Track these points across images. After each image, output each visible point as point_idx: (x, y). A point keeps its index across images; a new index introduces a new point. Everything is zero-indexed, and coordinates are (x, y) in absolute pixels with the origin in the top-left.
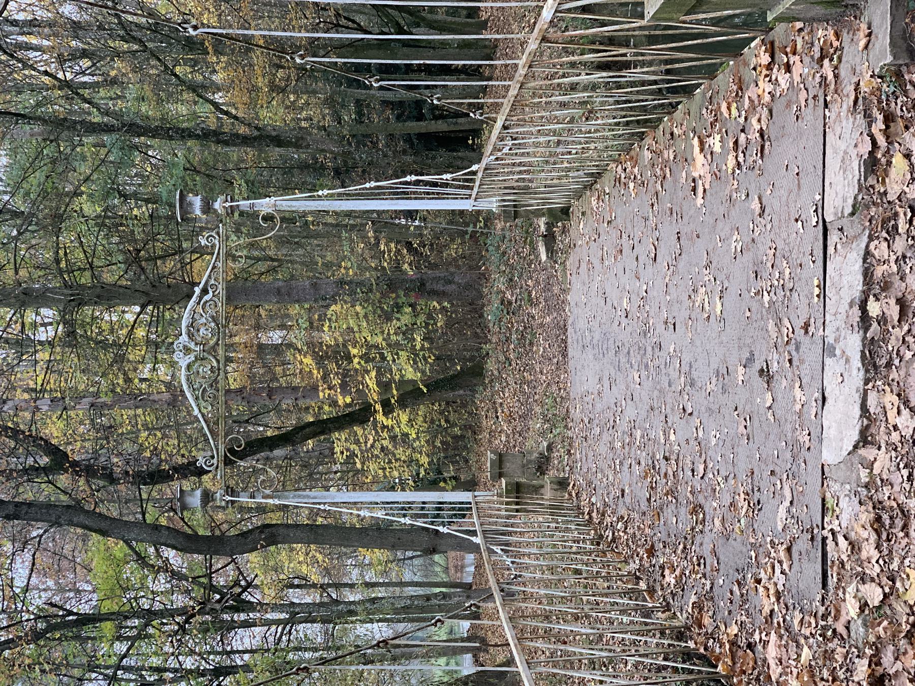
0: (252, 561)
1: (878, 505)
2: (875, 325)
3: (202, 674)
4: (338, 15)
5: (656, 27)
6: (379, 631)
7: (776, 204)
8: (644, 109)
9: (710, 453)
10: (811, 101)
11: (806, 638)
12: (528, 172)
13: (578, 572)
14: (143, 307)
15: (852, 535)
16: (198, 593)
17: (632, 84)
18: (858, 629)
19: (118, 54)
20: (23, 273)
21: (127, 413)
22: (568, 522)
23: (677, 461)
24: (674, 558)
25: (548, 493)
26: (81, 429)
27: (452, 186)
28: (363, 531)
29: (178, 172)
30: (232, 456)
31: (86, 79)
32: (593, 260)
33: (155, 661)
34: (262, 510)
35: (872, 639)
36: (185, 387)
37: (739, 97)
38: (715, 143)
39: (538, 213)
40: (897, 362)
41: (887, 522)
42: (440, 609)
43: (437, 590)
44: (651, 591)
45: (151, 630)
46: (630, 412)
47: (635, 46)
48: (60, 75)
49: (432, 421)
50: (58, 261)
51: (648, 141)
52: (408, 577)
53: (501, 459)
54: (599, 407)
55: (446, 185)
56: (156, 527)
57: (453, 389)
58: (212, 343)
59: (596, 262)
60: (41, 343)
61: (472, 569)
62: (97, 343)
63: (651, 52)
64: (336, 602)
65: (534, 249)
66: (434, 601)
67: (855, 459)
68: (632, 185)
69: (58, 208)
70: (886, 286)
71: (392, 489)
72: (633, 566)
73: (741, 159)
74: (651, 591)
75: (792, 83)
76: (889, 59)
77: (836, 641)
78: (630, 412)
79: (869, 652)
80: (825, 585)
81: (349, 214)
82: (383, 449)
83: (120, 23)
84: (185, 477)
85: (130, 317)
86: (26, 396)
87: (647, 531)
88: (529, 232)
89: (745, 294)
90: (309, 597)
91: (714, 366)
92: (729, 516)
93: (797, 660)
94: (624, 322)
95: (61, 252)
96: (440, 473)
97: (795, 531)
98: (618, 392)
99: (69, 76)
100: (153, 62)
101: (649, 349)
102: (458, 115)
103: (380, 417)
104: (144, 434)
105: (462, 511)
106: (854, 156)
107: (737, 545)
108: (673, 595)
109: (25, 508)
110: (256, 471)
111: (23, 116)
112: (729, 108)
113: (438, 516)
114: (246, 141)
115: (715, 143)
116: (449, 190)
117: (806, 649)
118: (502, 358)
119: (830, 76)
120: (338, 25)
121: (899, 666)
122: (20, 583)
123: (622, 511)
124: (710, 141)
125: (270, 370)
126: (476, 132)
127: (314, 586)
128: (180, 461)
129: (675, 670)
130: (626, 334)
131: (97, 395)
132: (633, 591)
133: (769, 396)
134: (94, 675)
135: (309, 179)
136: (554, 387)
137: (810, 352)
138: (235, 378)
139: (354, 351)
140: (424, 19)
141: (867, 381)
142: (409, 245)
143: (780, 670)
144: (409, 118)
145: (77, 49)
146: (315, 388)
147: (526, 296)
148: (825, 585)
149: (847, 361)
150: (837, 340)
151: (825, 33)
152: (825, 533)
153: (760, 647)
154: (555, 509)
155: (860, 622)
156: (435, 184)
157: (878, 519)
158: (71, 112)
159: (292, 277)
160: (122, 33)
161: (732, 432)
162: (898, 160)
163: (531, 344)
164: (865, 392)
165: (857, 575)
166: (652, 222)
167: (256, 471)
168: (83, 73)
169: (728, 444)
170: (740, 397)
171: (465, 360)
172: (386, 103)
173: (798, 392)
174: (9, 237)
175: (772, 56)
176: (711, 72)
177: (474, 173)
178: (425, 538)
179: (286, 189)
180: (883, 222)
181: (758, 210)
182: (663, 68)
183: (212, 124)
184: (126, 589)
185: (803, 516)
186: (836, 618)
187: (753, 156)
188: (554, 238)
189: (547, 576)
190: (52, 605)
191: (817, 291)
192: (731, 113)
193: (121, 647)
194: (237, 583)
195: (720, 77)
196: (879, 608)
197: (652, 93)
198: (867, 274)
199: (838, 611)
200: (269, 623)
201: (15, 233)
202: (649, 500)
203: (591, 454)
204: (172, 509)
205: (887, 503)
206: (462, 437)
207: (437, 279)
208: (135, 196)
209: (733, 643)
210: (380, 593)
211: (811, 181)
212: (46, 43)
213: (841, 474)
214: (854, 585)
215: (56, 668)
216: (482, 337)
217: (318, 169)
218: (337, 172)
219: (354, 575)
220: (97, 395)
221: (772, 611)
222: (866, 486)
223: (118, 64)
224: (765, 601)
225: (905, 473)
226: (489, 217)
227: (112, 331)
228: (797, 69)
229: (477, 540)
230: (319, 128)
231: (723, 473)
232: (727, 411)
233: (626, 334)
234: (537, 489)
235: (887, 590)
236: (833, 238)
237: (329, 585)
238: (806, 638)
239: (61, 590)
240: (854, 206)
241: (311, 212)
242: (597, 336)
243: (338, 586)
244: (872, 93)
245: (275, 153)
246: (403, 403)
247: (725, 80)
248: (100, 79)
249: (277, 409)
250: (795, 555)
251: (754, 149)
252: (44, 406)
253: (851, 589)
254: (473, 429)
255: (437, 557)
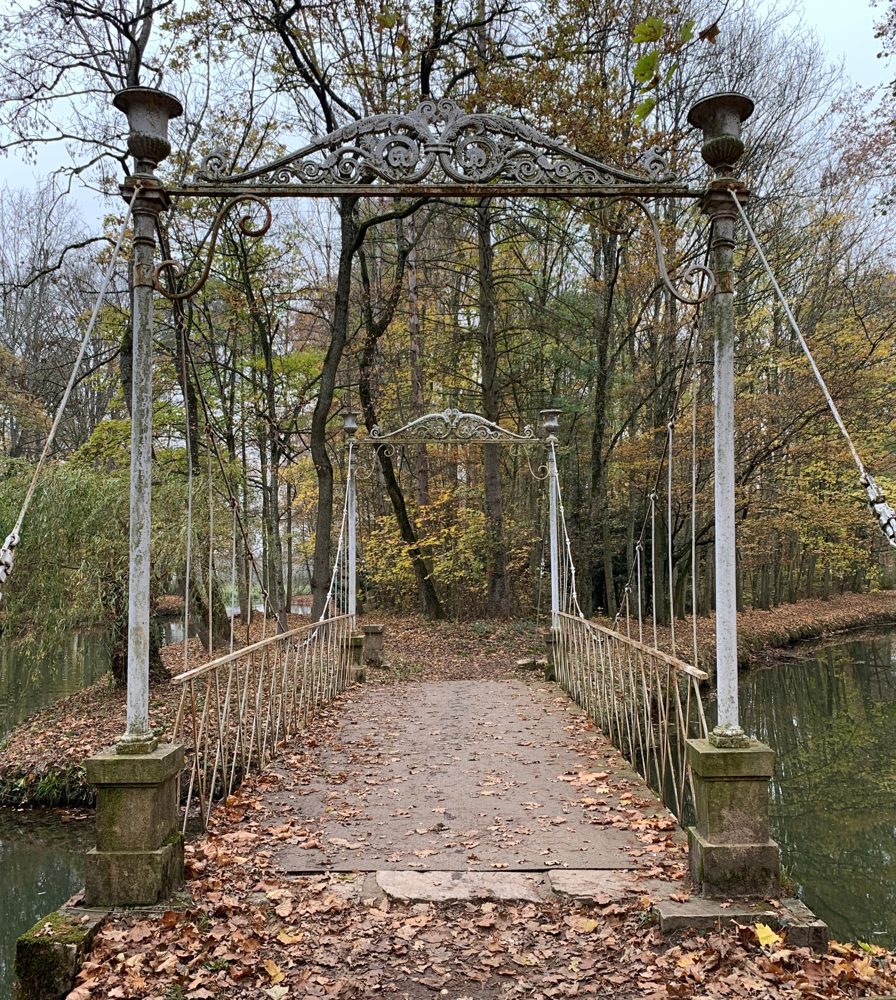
0: (307, 460)
1: (347, 912)
2: (476, 908)
3: (229, 428)
4: (684, 516)
5: (682, 747)
6: (257, 549)
7: (560, 834)
8: (625, 734)
9: (383, 788)
10: (633, 859)
11: (253, 860)
12: (579, 650)
13: (299, 690)
14: (482, 385)
15: (326, 894)
16: (286, 425)
17: (643, 726)
18: (259, 898)
19: (653, 367)
20: (504, 305)
21: (409, 375)
22: (334, 683)
23: (378, 763)
24: (308, 762)
25: (354, 668)
26: (397, 344)
27: (568, 596)
28: (327, 537)
29: (574, 409)
30: (382, 449)
31: (636, 344)
32: (519, 698)
33: (238, 394)
34: (343, 466)
35: (253, 909)
36: (427, 416)
37: (635, 805)
38: (603, 789)
39: (550, 659)
40: (449, 925)
41: (335, 919)
42: (273, 592)
43: (286, 588)
44: (285, 745)
45: (259, 392)
46: (411, 728)
47: (669, 727)
48: (639, 328)
49: (404, 584)
50: (512, 328)
51: (603, 739)
52: (295, 567)
53: (378, 633)
54: (415, 704)
55: (569, 592)
56: (331, 396)
57: (427, 598)
58: (457, 433)
59: (517, 702)
60: (456, 317)
61: (300, 613)
62: (457, 355)
63: (665, 738)
64: (278, 520)
65: (525, 655)
66: (278, 587)
67: (379, 895)
68: (572, 727)
69: (548, 328)
70: (503, 916)
71: (357, 556)
72: (303, 733)
73: (592, 808)
74: (285, 745)
75: (645, 844)
76: (664, 916)
77: (251, 882)
78: (411, 728)
79: (243, 906)
80: (291, 873)
81: (547, 524)
82: (385, 549)
83: (675, 369)
84: (365, 415)
85: (474, 376)
86: (420, 307)
87: (328, 742)
88: (536, 651)
89: (496, 812)
90: (281, 500)
91: (445, 790)
92: (339, 802)
93: (237, 854)
94: (475, 722)
95: (518, 331)
96: (368, 589)
97: (329, 851)
98: (426, 718)
99: (638, 334)
100: (649, 391)
101: (456, 741)
102: (619, 599)
103: (407, 548)
104: (394, 386)
105: (342, 606)
106: (595, 891)
107: (318, 809)
108: (282, 762)
109: (344, 308)
110: (369, 462)
111: (610, 304)
112: (627, 798)
113: (339, 588)
114: (597, 454)
115: (603, 789)
116: (565, 594)
117: (245, 860)
118: (449, 632)
119: (651, 873)
120: (678, 516)
121: (234, 928)
122: (292, 303)
123: (342, 723)
124: (604, 785)
125: (440, 470)
126: (606, 613)
127: (290, 504)
128: (377, 411)
129: (230, 761)
130: (467, 724)
131: (421, 355)
132: (285, 730)
133: (424, 831)
134: (229, 353)
135: (571, 497)
136: (429, 671)
137: (456, 861)
138: (432, 447)
139: (453, 529)
140: (684, 575)
141: (435, 903)
142: (527, 566)
143: (230, 841)
144: (615, 565)
145: (656, 339)
146: (426, 502)
147: (493, 649)
148: (291, 873)
149: (450, 888)
150: (464, 880)
151: (681, 868)
152: (327, 874)
153: (246, 826)
154: (343, 674)
155: (264, 899)
156: (569, 584)
157: (338, 913)
158: (613, 335)
159: (503, 486)
160: (668, 370)
161: (398, 804)
162: (592, 924)
163: (459, 653)
164: (428, 902)
165: (298, 897)
166: (545, 742)
167: (369, 462)
168: (640, 343)
169: (390, 801)
170: (424, 810)
171: (447, 607)
172: (625, 549)
173: (427, 852)
174: (527, 295)
175: (664, 830)
176: (652, 784)
177: (578, 615)
178: (322, 580)
179: (564, 481)
180: (548, 913)
181: (556, 821)
182: (655, 747)
183: (607, 431)
184: (288, 374)
185: (339, 857)
186: (267, 882)
187: (594, 817)
188: (533, 669)
189: (296, 668)
190: (277, 326)
191: (499, 865)
192: (623, 801)
193: (247, 373)
194: (291, 450)
195: (649, 792)
196: (275, 914)
197: (637, 740)
198: (511, 902)
199: (272, 883)
200: (263, 472)
201: (531, 299)
202: (349, 743)
203: (382, 699)
204: (343, 407)
205: (349, 919)
206: (394, 604)
207: (503, 586)
208: (557, 379)
209: (249, 806)
210: (284, 548)
211: (577, 859)
212: (660, 318)
213: (369, 884)
214: (290, 895)
215: (233, 329)
216: (464, 617)
217: (578, 503)
218: (576, 516)
219: (296, 530)
220: (421, 355)
221: (271, 835)
222: (361, 903)
223: (647, 366)
224: (278, 830)
225: (371, 932)
226: (547, 622)
227: (465, 365)
228: (655, 848)
229: (322, 619)
230: (606, 504)
231: (369, 798)
232: (413, 800)
233: (467, 724)
234: (357, 660)
235: (287, 919)
236: (537, 877)
237: (290, 514)
238: (253, 860)
239: (287, 330)
240: (559, 892)
241: (548, 498)
242: (465, 702)
243: (289, 520)
244: (639, 904)
245: (589, 473)
246: (417, 563)
247: (647, 795)
248: (636, 355)
249: (412, 476)
250: (311, 851)
251: (598, 817)
252: (414, 320)
253: (288, 893)
254: (399, 612)
255: (309, 587)
